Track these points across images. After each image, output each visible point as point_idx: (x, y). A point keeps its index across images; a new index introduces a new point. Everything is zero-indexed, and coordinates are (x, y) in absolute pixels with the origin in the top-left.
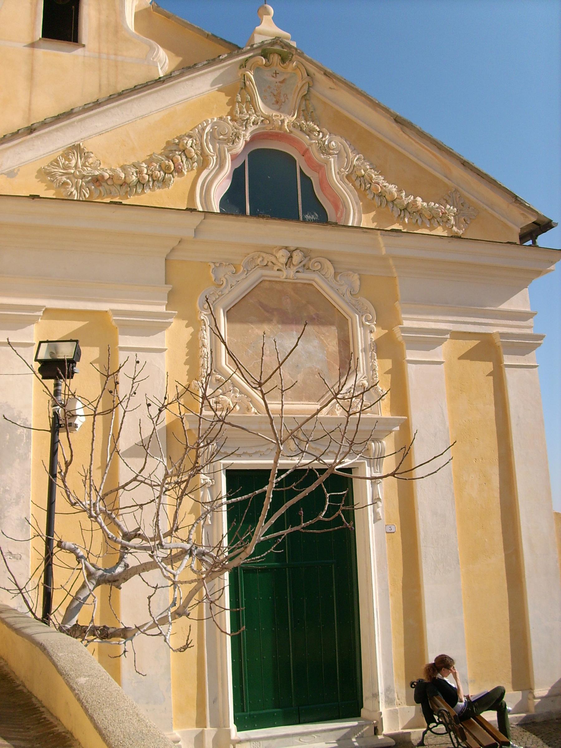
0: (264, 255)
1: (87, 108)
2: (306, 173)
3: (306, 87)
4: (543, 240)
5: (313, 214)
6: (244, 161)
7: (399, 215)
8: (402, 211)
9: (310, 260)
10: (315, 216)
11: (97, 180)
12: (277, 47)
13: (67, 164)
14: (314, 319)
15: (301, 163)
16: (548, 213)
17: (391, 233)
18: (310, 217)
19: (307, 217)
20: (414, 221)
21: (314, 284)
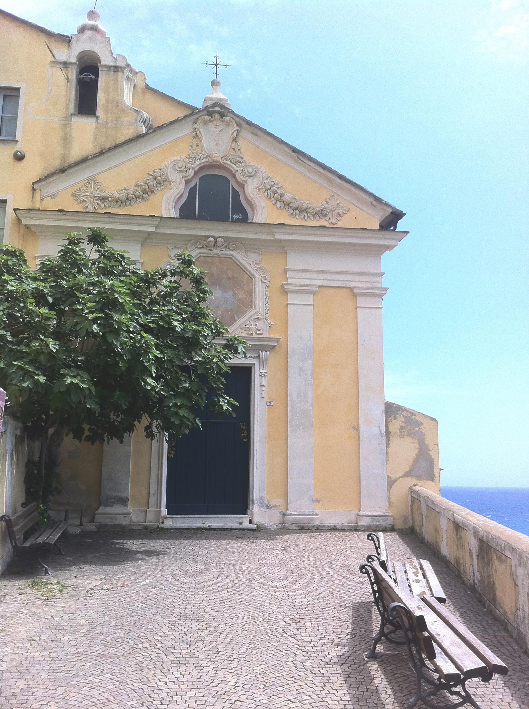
0: (201, 241)
1: (95, 156)
2: (236, 189)
3: (235, 134)
4: (401, 225)
5: (238, 215)
6: (197, 183)
7: (292, 214)
8: (294, 211)
9: (229, 243)
10: (240, 216)
11: (104, 199)
12: (217, 109)
13: (14, 265)
14: (231, 279)
15: (232, 183)
16: (399, 207)
17: (278, 226)
18: (236, 217)
19: (235, 217)
20: (302, 216)
21: (233, 257)
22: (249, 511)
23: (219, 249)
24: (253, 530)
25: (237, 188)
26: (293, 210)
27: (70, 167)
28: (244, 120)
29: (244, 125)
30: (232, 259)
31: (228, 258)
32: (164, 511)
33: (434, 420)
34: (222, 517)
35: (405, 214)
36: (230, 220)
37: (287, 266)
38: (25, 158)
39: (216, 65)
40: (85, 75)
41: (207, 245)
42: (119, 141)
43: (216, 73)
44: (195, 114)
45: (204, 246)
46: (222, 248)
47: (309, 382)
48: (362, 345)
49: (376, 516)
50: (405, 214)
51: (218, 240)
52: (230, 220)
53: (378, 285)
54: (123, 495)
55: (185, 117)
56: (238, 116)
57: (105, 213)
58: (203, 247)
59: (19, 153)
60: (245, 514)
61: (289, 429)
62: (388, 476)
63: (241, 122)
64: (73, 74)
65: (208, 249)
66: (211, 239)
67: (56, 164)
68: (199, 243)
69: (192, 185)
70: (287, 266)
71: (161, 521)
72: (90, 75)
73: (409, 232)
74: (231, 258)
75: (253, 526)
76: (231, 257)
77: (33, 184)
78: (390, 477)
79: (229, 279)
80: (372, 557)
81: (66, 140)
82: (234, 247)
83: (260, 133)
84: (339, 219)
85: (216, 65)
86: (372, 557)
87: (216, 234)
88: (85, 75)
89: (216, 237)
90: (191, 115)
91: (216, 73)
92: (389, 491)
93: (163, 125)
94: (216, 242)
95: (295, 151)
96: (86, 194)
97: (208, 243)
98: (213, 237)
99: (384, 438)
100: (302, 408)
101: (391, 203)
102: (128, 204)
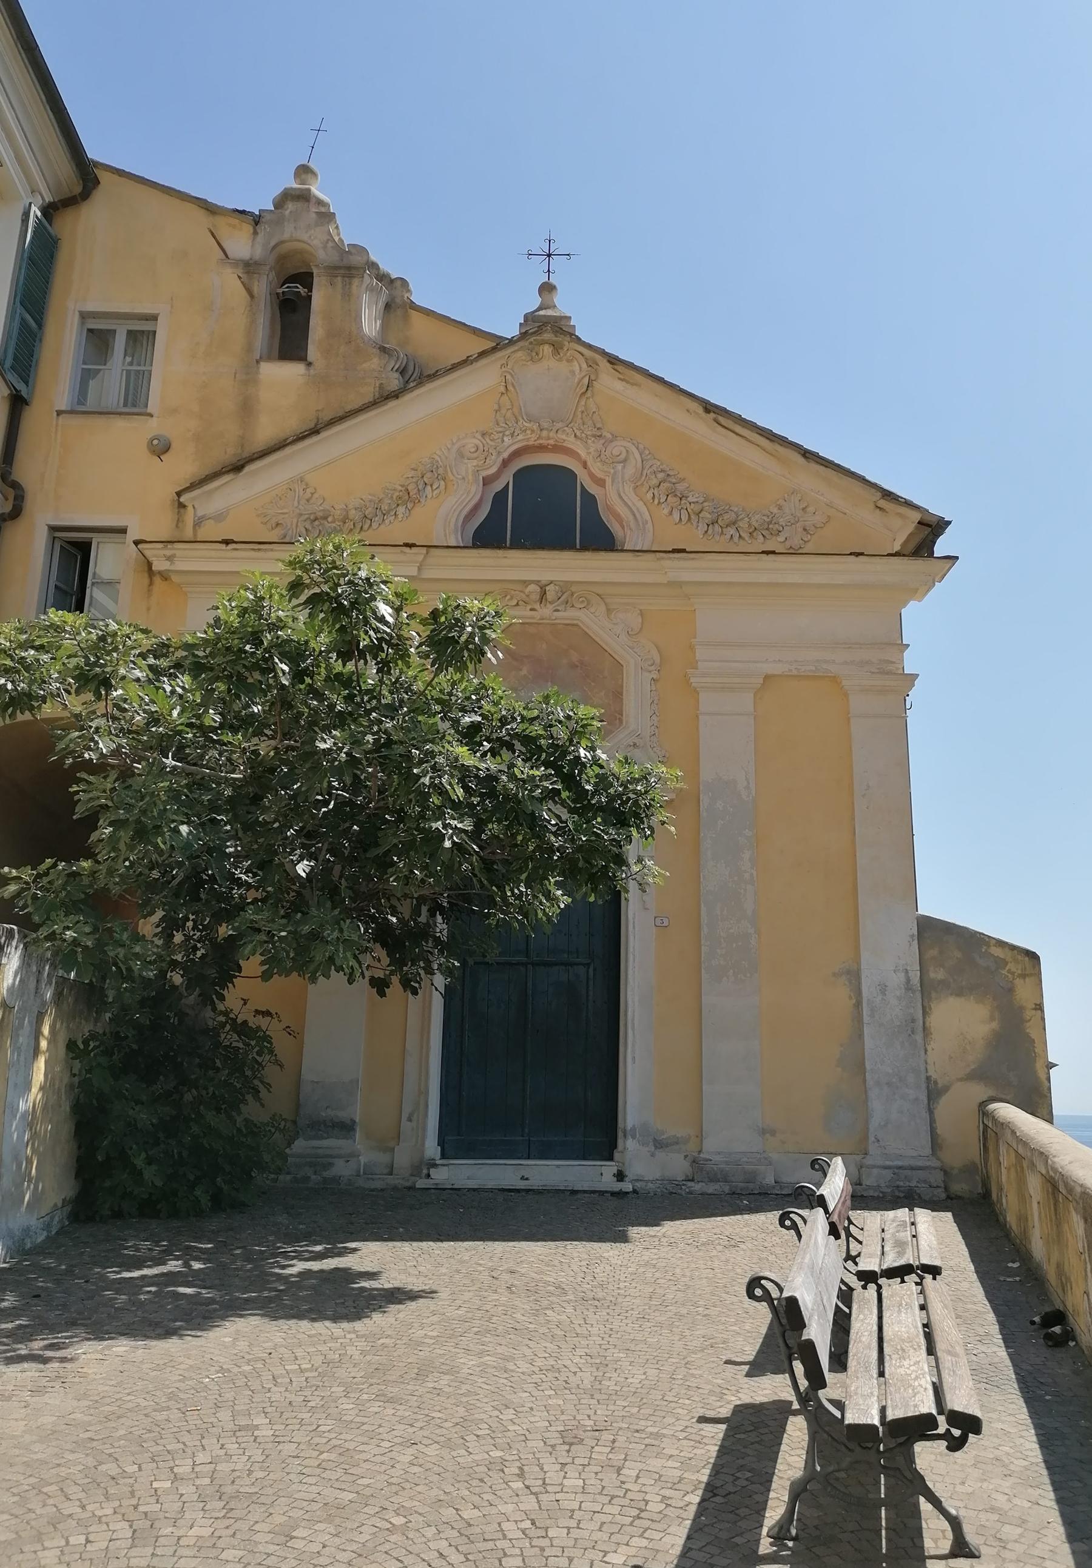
4: (941, 548)
7: (706, 532)
8: (711, 526)
9: (572, 595)
14: (577, 666)
16: (937, 509)
17: (671, 555)
22: (616, 1155)
23: (551, 607)
24: (620, 1195)
25: (593, 489)
26: (708, 525)
27: (251, 460)
28: (603, 353)
29: (603, 363)
30: (580, 627)
31: (573, 625)
32: (432, 1148)
33: (1033, 957)
34: (558, 1166)
35: (949, 523)
36: (578, 547)
37: (695, 638)
38: (173, 445)
39: (549, 255)
40: (288, 287)
41: (526, 599)
42: (348, 408)
43: (549, 271)
44: (501, 349)
45: (520, 602)
46: (558, 605)
47: (747, 876)
48: (864, 796)
49: (900, 1168)
50: (949, 523)
51: (547, 588)
52: (578, 547)
53: (891, 667)
54: (343, 1115)
55: (483, 354)
56: (590, 347)
57: (671, 584)
58: (517, 604)
59: (155, 442)
60: (610, 1158)
61: (704, 975)
62: (928, 1078)
63: (598, 357)
64: (262, 286)
65: (529, 607)
66: (532, 588)
67: (228, 453)
68: (508, 597)
69: (498, 486)
70: (695, 638)
71: (425, 1171)
72: (298, 288)
73: (957, 558)
74: (577, 625)
75: (627, 1186)
76: (575, 622)
77: (179, 494)
78: (936, 1082)
79: (574, 666)
80: (763, 1282)
81: (247, 409)
82: (583, 601)
83: (638, 377)
84: (806, 539)
85: (549, 255)
86: (763, 1282)
87: (545, 577)
88: (288, 287)
89: (544, 583)
90: (494, 349)
91: (549, 271)
92: (931, 1112)
93: (437, 371)
94: (544, 593)
95: (709, 407)
96: (285, 511)
97: (528, 596)
98: (537, 582)
99: (918, 995)
100: (732, 931)
101: (917, 501)
102: (366, 527)
